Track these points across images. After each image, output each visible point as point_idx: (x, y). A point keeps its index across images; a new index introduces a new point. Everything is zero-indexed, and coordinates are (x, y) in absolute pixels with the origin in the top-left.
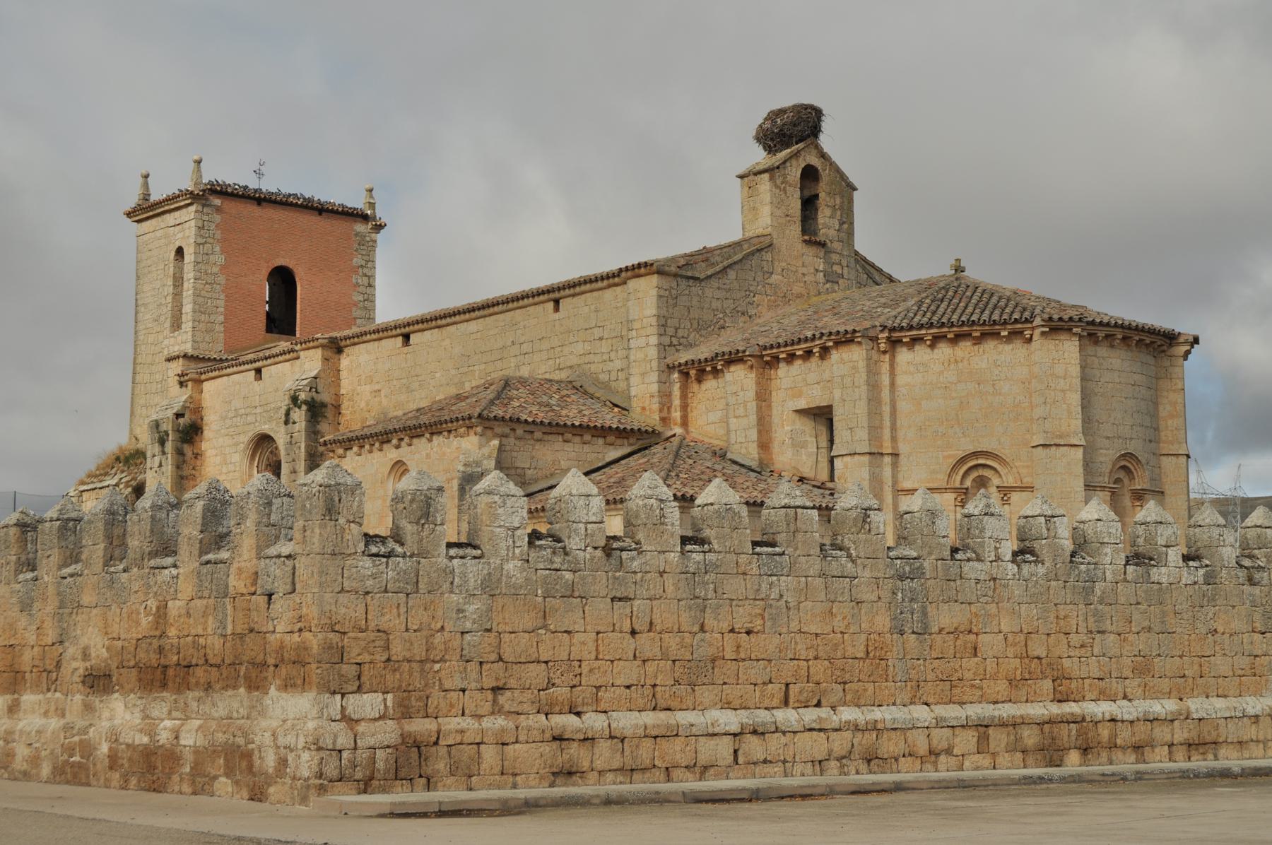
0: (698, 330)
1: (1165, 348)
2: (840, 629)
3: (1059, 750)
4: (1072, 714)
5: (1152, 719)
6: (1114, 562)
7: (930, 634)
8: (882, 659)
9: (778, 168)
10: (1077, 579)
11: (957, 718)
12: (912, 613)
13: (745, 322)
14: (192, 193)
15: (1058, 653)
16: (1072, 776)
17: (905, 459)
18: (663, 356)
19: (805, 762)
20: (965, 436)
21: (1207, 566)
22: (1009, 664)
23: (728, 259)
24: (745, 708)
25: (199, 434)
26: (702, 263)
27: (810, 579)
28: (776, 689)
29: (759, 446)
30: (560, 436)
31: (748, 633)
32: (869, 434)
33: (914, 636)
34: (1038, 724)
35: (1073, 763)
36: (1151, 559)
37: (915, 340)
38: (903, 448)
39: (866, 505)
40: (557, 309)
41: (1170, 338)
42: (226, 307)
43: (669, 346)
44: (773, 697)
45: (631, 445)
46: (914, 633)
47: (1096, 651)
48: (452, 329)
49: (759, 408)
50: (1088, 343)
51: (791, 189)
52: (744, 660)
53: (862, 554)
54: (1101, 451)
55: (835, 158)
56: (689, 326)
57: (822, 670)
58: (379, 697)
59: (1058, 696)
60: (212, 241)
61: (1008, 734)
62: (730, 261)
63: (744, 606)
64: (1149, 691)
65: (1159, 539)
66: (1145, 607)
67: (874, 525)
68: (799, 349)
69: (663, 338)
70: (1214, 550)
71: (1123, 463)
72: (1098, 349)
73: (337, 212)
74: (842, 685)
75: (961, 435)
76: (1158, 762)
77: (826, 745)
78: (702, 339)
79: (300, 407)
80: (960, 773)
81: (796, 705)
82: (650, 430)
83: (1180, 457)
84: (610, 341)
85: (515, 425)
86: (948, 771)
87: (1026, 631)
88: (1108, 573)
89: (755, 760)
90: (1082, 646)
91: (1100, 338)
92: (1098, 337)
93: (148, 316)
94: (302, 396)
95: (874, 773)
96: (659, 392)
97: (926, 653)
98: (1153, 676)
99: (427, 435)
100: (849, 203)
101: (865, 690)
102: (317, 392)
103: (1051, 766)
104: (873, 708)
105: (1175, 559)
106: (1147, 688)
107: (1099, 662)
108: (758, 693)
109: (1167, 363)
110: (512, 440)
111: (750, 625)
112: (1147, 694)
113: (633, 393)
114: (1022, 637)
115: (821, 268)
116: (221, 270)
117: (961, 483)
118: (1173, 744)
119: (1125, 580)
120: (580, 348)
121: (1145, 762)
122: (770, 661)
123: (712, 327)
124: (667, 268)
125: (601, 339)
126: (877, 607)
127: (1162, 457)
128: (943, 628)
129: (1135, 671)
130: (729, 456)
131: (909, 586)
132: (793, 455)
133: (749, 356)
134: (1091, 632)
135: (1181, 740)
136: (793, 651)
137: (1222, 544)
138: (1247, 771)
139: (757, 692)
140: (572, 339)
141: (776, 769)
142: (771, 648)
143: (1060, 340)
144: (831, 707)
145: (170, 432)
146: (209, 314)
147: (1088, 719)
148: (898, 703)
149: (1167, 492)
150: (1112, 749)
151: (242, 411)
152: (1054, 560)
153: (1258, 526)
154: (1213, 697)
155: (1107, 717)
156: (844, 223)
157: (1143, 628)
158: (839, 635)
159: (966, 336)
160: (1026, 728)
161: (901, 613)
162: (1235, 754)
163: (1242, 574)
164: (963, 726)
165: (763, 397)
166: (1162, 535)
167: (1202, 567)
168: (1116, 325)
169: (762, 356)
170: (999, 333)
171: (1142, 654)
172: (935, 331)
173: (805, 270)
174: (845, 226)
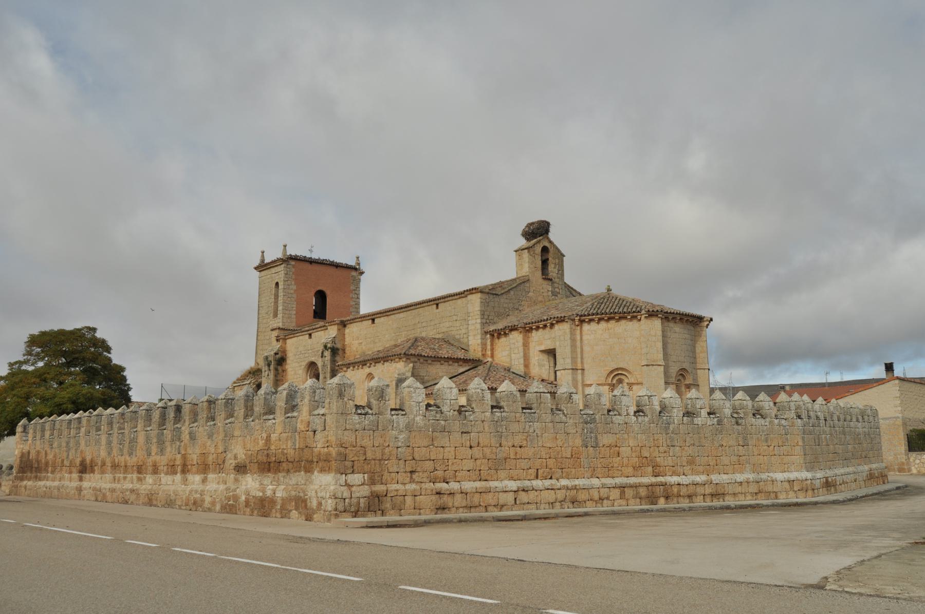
0: (498, 316)
1: (698, 323)
7: (599, 447)
9: (531, 247)
11: (611, 484)
12: (591, 438)
14: (282, 259)
21: (718, 417)
24: (519, 480)
28: (532, 472)
34: (646, 486)
36: (694, 414)
37: (591, 320)
38: (586, 367)
42: (297, 307)
46: (592, 447)
47: (671, 454)
48: (392, 316)
52: (519, 459)
53: (569, 413)
58: (361, 475)
59: (655, 474)
67: (574, 400)
71: (681, 373)
79: (328, 350)
81: (541, 478)
84: (460, 321)
88: (675, 420)
94: (329, 345)
96: (481, 343)
101: (571, 472)
102: (335, 344)
103: (652, 505)
107: (672, 459)
110: (418, 364)
118: (705, 495)
119: (683, 423)
120: (447, 324)
121: (693, 502)
122: (530, 459)
124: (484, 290)
125: (456, 320)
127: (698, 370)
130: (511, 370)
134: (668, 446)
135: (709, 493)
140: (444, 321)
142: (530, 454)
145: (272, 361)
147: (668, 484)
148: (585, 477)
149: (700, 385)
153: (741, 400)
157: (691, 444)
159: (613, 318)
161: (586, 438)
162: (732, 499)
163: (733, 420)
164: (614, 487)
165: (526, 345)
168: (677, 313)
169: (525, 328)
172: (600, 316)
173: (543, 291)
174: (560, 272)
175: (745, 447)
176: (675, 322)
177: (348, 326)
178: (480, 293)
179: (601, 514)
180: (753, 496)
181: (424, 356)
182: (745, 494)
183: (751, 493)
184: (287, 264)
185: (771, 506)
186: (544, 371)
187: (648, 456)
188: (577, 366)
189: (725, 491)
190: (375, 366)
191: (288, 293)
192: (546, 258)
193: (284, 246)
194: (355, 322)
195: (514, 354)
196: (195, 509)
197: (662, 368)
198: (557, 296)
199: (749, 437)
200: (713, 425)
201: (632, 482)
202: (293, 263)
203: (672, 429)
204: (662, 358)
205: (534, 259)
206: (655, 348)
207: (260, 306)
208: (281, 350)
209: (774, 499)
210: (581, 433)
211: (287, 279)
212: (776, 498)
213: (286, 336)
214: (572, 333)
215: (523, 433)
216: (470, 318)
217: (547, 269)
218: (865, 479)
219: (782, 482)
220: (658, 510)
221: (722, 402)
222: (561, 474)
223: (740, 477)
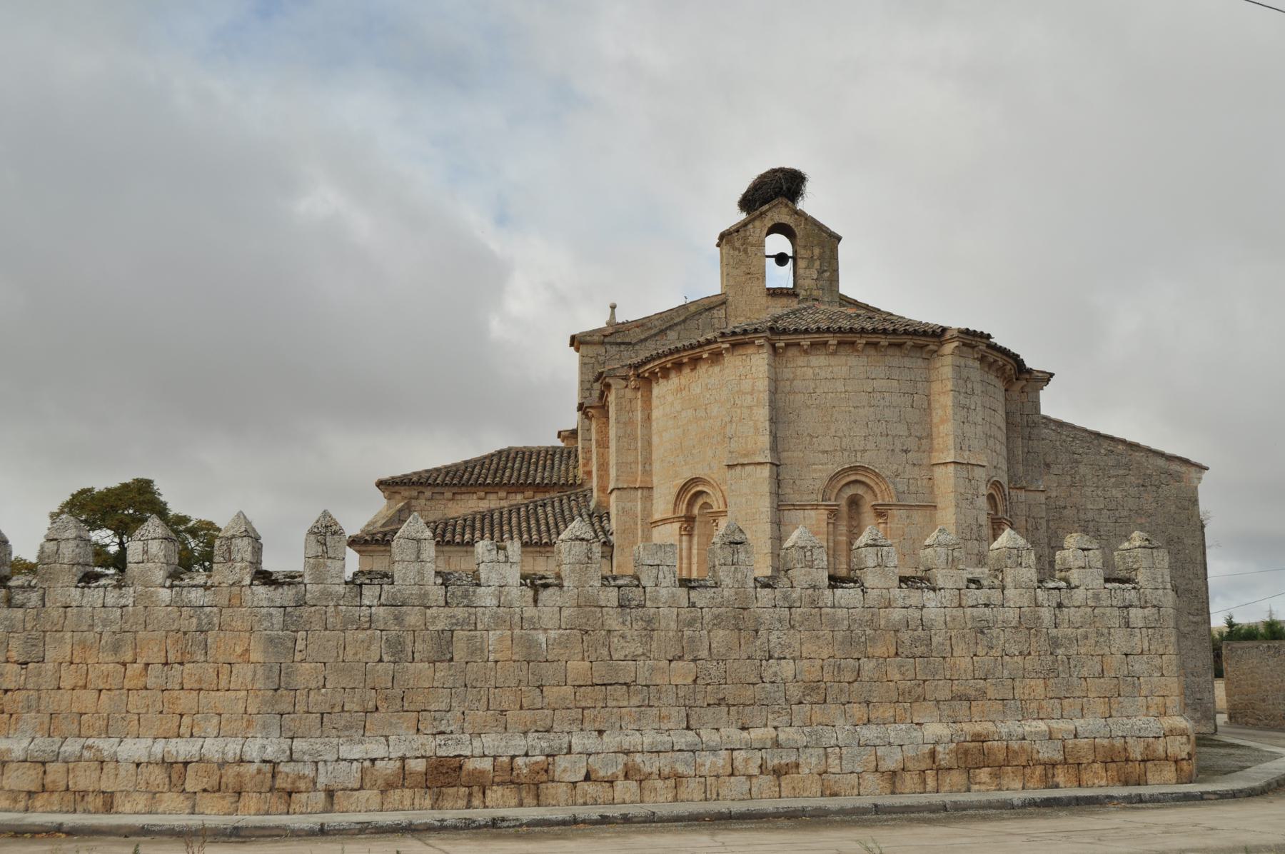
26: (637, 329)
50: (798, 354)
51: (754, 248)
54: (814, 467)
72: (812, 358)
85: (421, 488)
117: (674, 513)
127: (936, 468)
143: (747, 355)
149: (939, 505)
168: (906, 332)
174: (827, 274)
180: (15, 801)
183: (11, 791)
193: (611, 307)
197: (766, 472)
204: (768, 446)
206: (751, 423)
219: (138, 765)
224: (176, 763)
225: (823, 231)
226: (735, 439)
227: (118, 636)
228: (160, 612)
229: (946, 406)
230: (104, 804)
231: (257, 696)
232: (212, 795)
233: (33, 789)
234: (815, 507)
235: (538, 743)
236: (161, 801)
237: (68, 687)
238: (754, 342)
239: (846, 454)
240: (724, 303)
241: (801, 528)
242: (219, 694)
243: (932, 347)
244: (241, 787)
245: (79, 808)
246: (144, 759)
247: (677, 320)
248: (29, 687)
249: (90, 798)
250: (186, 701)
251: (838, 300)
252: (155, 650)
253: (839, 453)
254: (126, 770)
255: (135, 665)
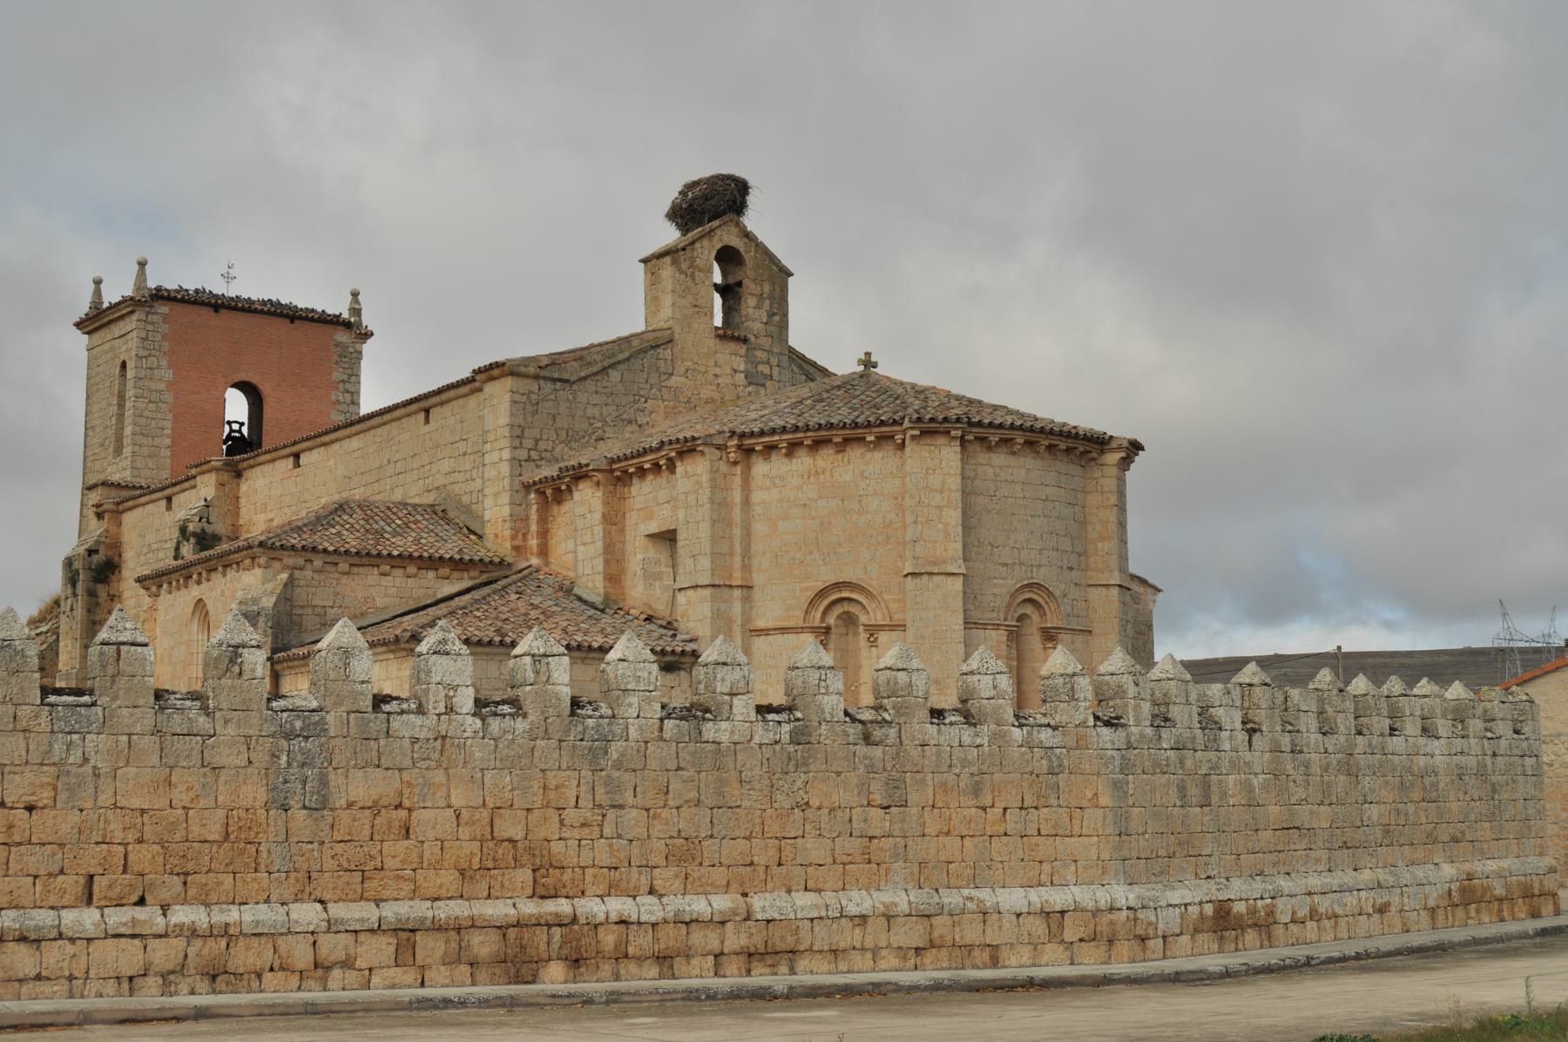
0: (567, 442)
1: (1094, 455)
2: (183, 804)
3: (531, 962)
4: (556, 914)
5: (688, 920)
6: (642, 715)
7: (332, 810)
8: (250, 843)
9: (684, 249)
10: (580, 737)
11: (362, 920)
12: (304, 783)
13: (632, 432)
14: (132, 299)
15: (543, 834)
16: (501, 998)
17: (760, 593)
18: (518, 472)
19: (104, 979)
20: (825, 564)
21: (798, 720)
22: (461, 848)
23: (610, 358)
24: (16, 907)
25: (117, 572)
26: (573, 363)
27: (135, 737)
28: (71, 883)
29: (605, 579)
30: (376, 569)
31: (30, 808)
32: (712, 562)
33: (304, 812)
34: (500, 927)
35: (554, 978)
36: (707, 711)
37: (770, 448)
38: (758, 579)
39: (237, 640)
40: (427, 421)
41: (1097, 443)
42: (173, 429)
43: (526, 461)
44: (65, 892)
45: (472, 578)
46: (305, 807)
47: (607, 831)
48: (336, 446)
49: (607, 534)
51: (701, 274)
52: (20, 844)
53: (224, 705)
54: (995, 581)
55: (761, 238)
56: (555, 437)
57: (149, 856)
59: (540, 891)
60: (157, 353)
61: (447, 941)
62: (612, 361)
63: (22, 773)
64: (693, 883)
65: (719, 685)
66: (692, 773)
67: (246, 667)
68: (646, 462)
69: (518, 451)
70: (808, 699)
71: (1027, 596)
73: (312, 320)
74: (182, 876)
75: (821, 562)
76: (697, 977)
77: (141, 956)
78: (573, 453)
79: (188, 541)
80: (365, 993)
81: (102, 903)
82: (497, 560)
83: (1111, 589)
84: (472, 456)
85: (310, 556)
86: (344, 989)
87: (491, 806)
88: (632, 730)
89: (21, 975)
90: (583, 825)
91: (993, 443)
92: (990, 441)
93: (95, 440)
94: (191, 527)
95: (220, 993)
96: (511, 515)
97: (324, 834)
98: (701, 864)
99: (220, 569)
100: (782, 290)
101: (219, 884)
102: (208, 522)
103: (516, 983)
104: (231, 906)
105: (744, 710)
106: (690, 879)
107: (611, 846)
108: (39, 888)
109: (1097, 474)
110: (308, 573)
111: (31, 798)
112: (689, 887)
113: (486, 518)
114: (485, 814)
115: (742, 367)
116: (167, 387)
118: (722, 953)
119: (662, 739)
120: (446, 466)
121: (674, 977)
122: (62, 845)
123: (587, 439)
124: (522, 369)
125: (465, 454)
126: (246, 774)
127: (1090, 589)
128: (354, 802)
129: (670, 858)
130: (576, 590)
131: (300, 747)
132: (645, 589)
133: (594, 470)
134: (600, 806)
135: (737, 948)
136: (101, 832)
137: (823, 691)
138: (798, 990)
139: (38, 886)
140: (440, 455)
141: (55, 988)
142: (65, 829)
143: (936, 446)
144: (162, 907)
145: (81, 571)
146: (153, 437)
147: (582, 921)
148: (273, 898)
149: (1096, 631)
150: (620, 961)
151: (155, 546)
152: (543, 712)
153: (890, 668)
154: (798, 891)
155: (614, 917)
156: (774, 314)
157: (686, 801)
158: (180, 812)
159: (826, 442)
160: (477, 933)
161: (286, 782)
162: (825, 966)
163: (854, 731)
164: (372, 931)
165: (613, 520)
166: (723, 680)
167: (789, 721)
169: (612, 471)
170: (864, 438)
171: (683, 834)
172: (790, 436)
173: (718, 371)
174: (777, 318)
175: (894, 810)
176: (1014, 453)
177: (246, 474)
178: (510, 378)
179: (260, 1015)
180: (905, 958)
181: (325, 551)
182: (875, 951)
183: (900, 948)
184: (148, 313)
185: (927, 988)
186: (658, 591)
187: (520, 836)
188: (730, 577)
189: (797, 941)
190: (208, 580)
191: (151, 391)
192: (737, 279)
194: (260, 464)
195: (584, 544)
196: (1190, 908)
197: (958, 584)
198: (764, 385)
199: (908, 780)
200: (776, 742)
201: (443, 916)
202: (164, 309)
203: (615, 756)
205: (690, 283)
207: (89, 425)
208: (108, 541)
209: (985, 967)
210: (264, 765)
211: (147, 353)
212: (995, 962)
213: (118, 504)
214: (718, 486)
215: (42, 764)
216: (488, 446)
217: (738, 310)
218: (1431, 903)
219: (1018, 915)
220: (487, 1001)
221: (814, 676)
222: (180, 888)
223: (858, 901)
224: (1053, 912)
225: (774, 263)
226: (921, 543)
227: (976, 778)
228: (1016, 752)
229: (1107, 522)
230: (992, 957)
231: (1108, 842)
232: (1088, 944)
233: (921, 945)
234: (997, 626)
235: (1258, 886)
236: (1042, 952)
237: (934, 834)
238: (949, 432)
239: (1024, 568)
240: (671, 341)
241: (982, 648)
242: (1073, 840)
243: (1094, 455)
244: (1114, 935)
245: (967, 963)
246: (1025, 910)
247: (621, 357)
248: (895, 834)
249: (977, 952)
250: (1046, 847)
251: (787, 352)
252: (1013, 793)
253: (1017, 567)
254: (1009, 921)
255: (995, 810)
